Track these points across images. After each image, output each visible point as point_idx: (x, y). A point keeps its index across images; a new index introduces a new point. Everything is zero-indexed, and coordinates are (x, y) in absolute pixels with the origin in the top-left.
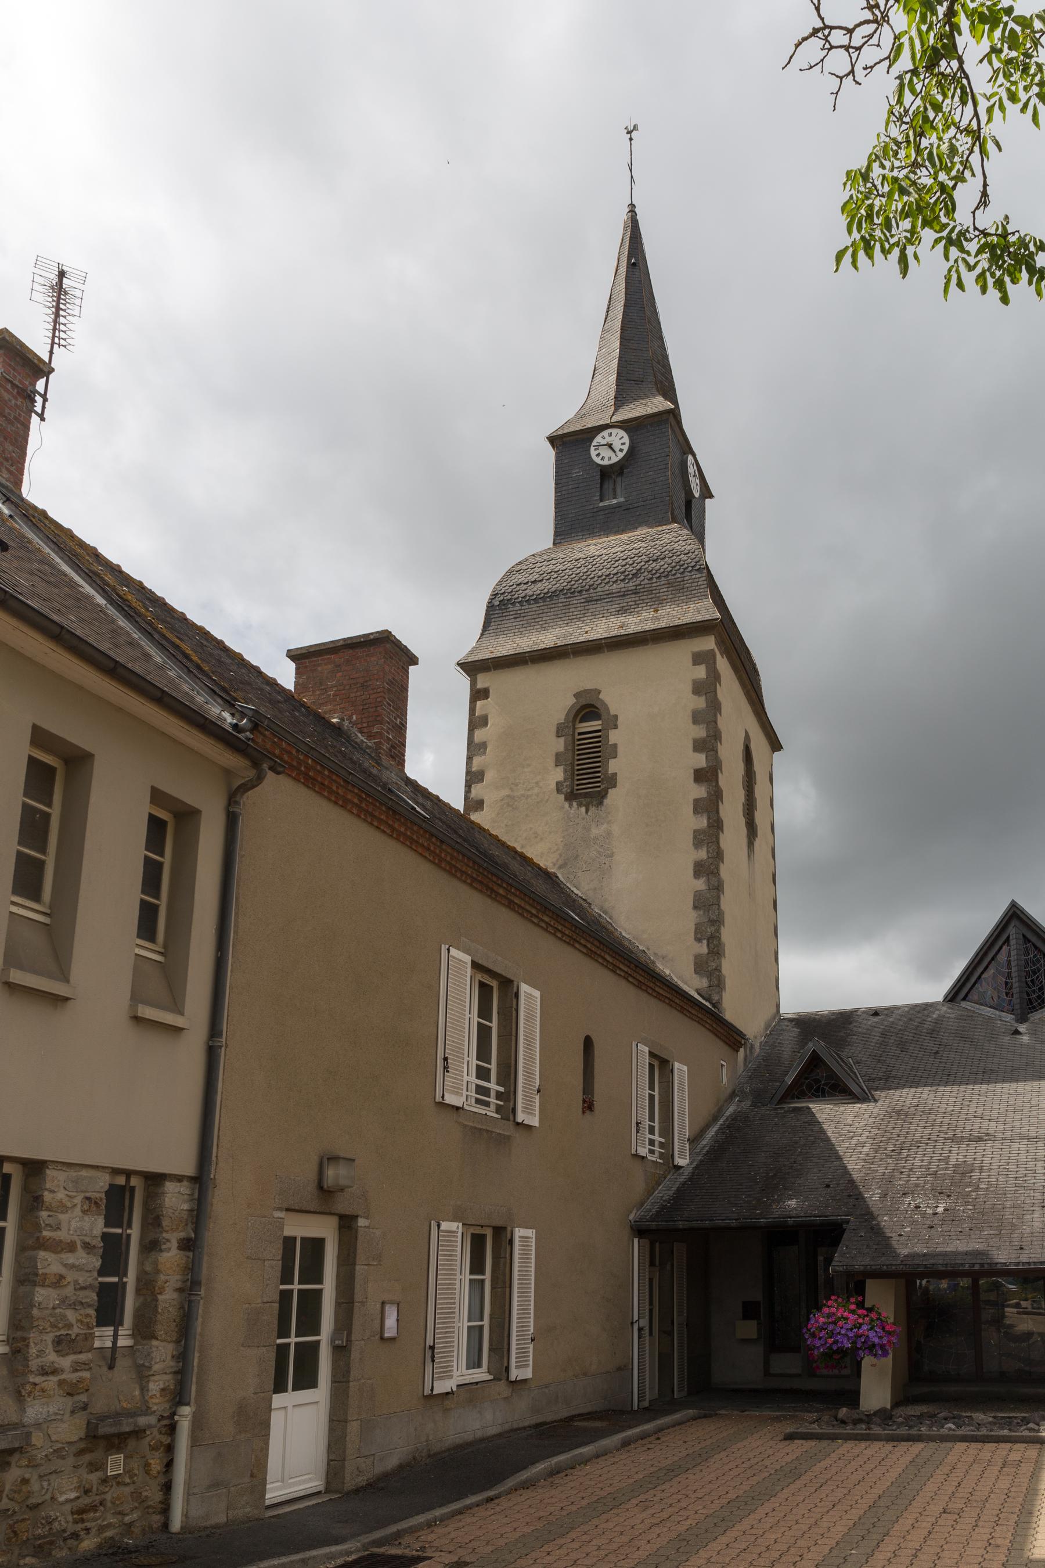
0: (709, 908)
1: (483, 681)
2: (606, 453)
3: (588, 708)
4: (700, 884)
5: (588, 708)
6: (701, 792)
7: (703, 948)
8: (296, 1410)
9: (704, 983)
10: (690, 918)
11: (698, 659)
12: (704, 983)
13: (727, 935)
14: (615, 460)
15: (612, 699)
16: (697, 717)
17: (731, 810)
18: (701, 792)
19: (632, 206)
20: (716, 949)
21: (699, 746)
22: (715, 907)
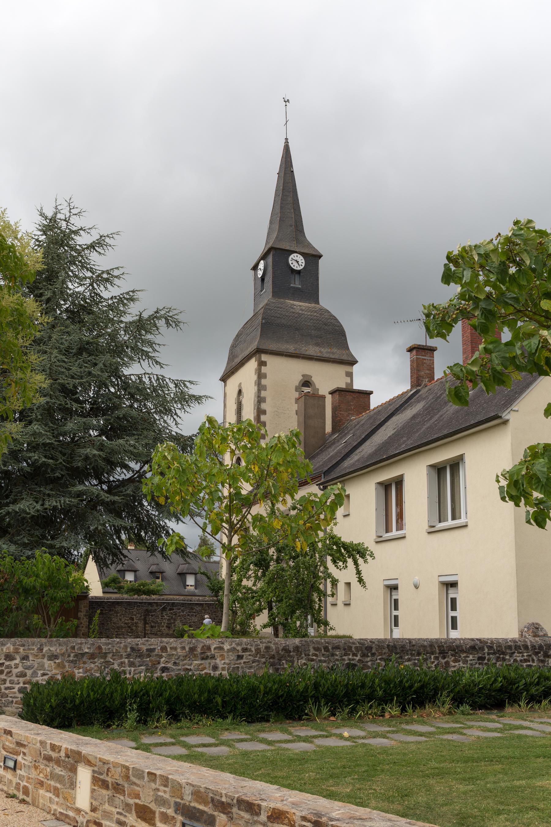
2: (296, 264)
3: (307, 383)
19: (286, 139)
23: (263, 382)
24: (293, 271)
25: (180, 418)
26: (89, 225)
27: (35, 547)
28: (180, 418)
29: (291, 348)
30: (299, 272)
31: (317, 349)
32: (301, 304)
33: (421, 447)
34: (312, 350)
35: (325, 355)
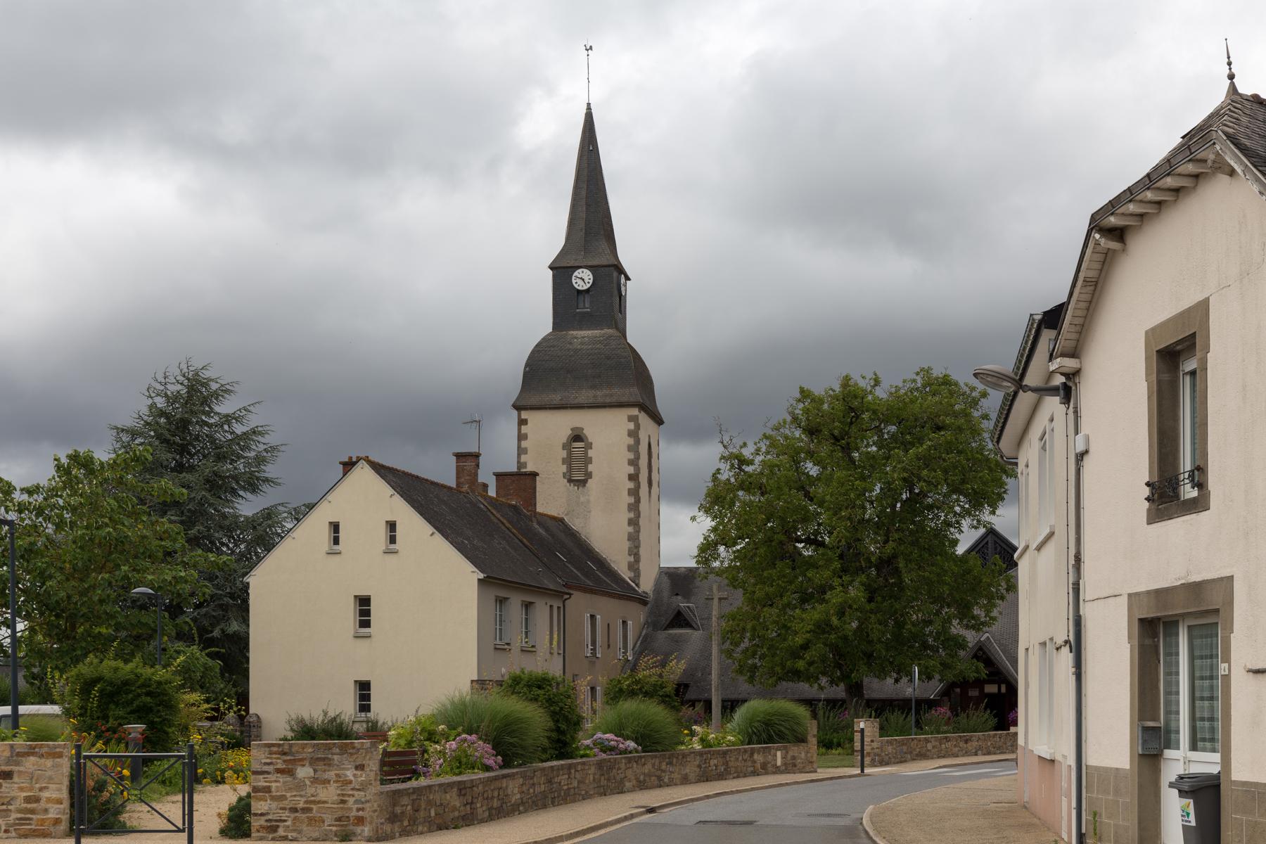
0: (634, 539)
1: (524, 415)
2: (580, 282)
3: (577, 437)
4: (631, 529)
5: (577, 437)
6: (631, 485)
7: (632, 559)
8: (374, 703)
9: (632, 575)
10: (626, 545)
11: (631, 419)
12: (632, 575)
13: (642, 551)
14: (585, 288)
15: (588, 433)
16: (630, 448)
17: (643, 462)
18: (631, 485)
19: (589, 104)
20: (637, 560)
21: (631, 463)
22: (656, 782)
23: (524, 444)
24: (579, 292)
25: (1044, 448)
26: (217, 373)
27: (154, 469)
28: (1044, 448)
29: (556, 398)
30: (588, 291)
31: (591, 393)
32: (590, 332)
33: (1193, 443)
34: (585, 396)
35: (600, 400)
